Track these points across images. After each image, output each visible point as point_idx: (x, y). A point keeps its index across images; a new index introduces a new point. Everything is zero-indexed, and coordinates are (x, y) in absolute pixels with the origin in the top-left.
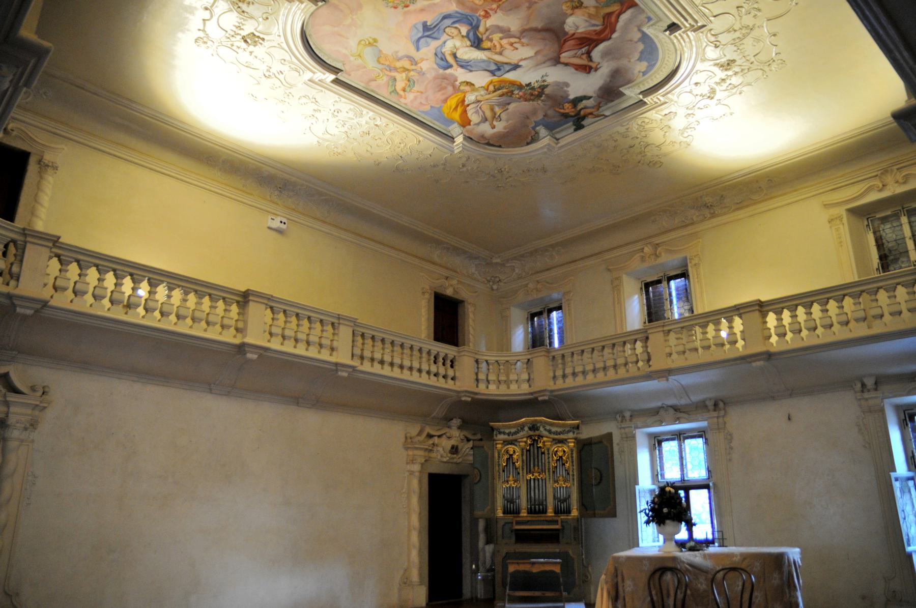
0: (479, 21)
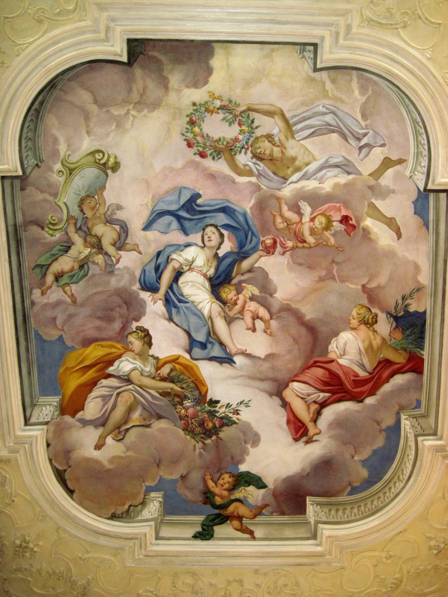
0: (255, 249)
